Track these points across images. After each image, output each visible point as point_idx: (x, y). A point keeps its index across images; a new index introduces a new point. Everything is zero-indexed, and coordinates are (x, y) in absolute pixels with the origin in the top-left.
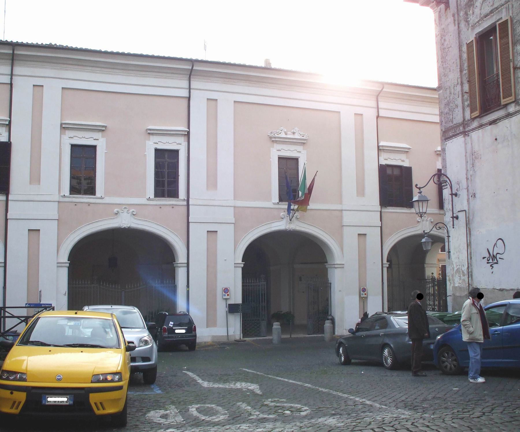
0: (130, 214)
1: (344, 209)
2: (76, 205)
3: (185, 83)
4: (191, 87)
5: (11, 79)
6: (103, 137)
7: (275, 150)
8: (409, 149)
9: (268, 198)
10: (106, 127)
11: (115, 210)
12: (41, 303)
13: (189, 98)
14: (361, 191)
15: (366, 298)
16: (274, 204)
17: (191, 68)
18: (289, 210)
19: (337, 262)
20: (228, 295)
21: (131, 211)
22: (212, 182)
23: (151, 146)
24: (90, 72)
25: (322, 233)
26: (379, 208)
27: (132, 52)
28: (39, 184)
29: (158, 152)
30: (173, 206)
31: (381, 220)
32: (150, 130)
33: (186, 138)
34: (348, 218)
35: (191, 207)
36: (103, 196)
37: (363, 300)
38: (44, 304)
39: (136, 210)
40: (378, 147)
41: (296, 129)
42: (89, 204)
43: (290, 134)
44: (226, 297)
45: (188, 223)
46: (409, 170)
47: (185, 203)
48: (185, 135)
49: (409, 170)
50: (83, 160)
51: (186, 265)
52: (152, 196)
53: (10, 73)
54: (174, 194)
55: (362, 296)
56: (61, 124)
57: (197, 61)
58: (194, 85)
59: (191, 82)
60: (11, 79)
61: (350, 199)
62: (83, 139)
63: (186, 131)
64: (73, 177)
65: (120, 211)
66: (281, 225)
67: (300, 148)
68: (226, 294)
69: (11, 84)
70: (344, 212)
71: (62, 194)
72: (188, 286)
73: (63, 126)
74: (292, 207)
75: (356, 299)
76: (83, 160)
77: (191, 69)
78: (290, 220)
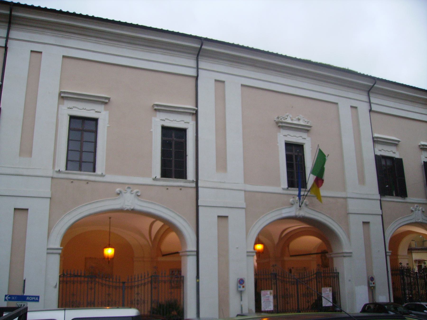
0: (133, 195)
1: (348, 196)
2: (72, 182)
3: (192, 63)
4: (199, 67)
5: (7, 41)
6: (105, 110)
7: (282, 136)
8: (399, 141)
9: (278, 184)
10: (109, 99)
11: (118, 190)
12: (25, 294)
13: (197, 78)
14: (362, 180)
15: (374, 287)
16: (284, 189)
17: (199, 46)
18: (299, 195)
19: (346, 249)
20: (243, 287)
21: (135, 191)
22: (222, 164)
23: (159, 121)
24: (94, 43)
25: (330, 220)
26: (378, 196)
27: (140, 24)
28: (31, 157)
29: (165, 129)
30: (181, 188)
31: (381, 208)
32: (157, 105)
33: (194, 117)
34: (353, 206)
35: (200, 189)
36: (104, 174)
37: (372, 289)
38: (29, 296)
39: (141, 191)
40: (373, 138)
41: (301, 116)
42: (88, 182)
43: (295, 120)
44: (241, 289)
45: (197, 206)
46: (399, 162)
47: (194, 185)
48: (193, 114)
49: (399, 162)
50: (82, 130)
51: (195, 253)
52: (159, 176)
53: (5, 36)
54: (182, 174)
55: (371, 285)
56: (61, 93)
57: (206, 40)
58: (202, 65)
59: (199, 62)
60: (7, 41)
61: (353, 188)
62: (83, 110)
63: (194, 109)
64: (95, 132)
65: (123, 191)
66: (292, 212)
67: (304, 135)
68: (242, 286)
69: (6, 48)
70: (348, 199)
71: (57, 169)
72: (198, 277)
73: (62, 95)
74: (302, 193)
75: (365, 289)
76: (82, 130)
77: (201, 48)
78: (300, 206)
